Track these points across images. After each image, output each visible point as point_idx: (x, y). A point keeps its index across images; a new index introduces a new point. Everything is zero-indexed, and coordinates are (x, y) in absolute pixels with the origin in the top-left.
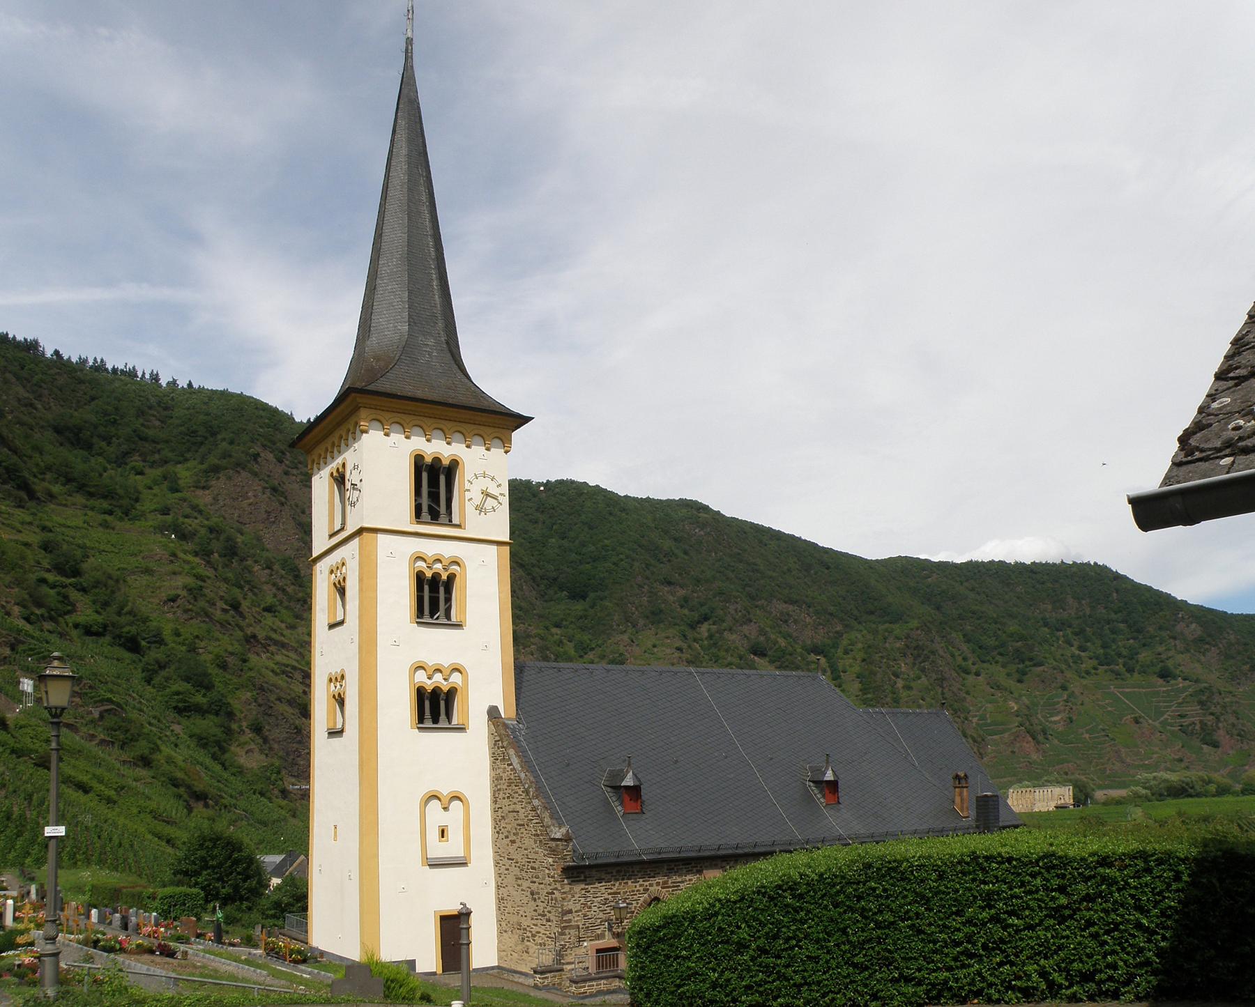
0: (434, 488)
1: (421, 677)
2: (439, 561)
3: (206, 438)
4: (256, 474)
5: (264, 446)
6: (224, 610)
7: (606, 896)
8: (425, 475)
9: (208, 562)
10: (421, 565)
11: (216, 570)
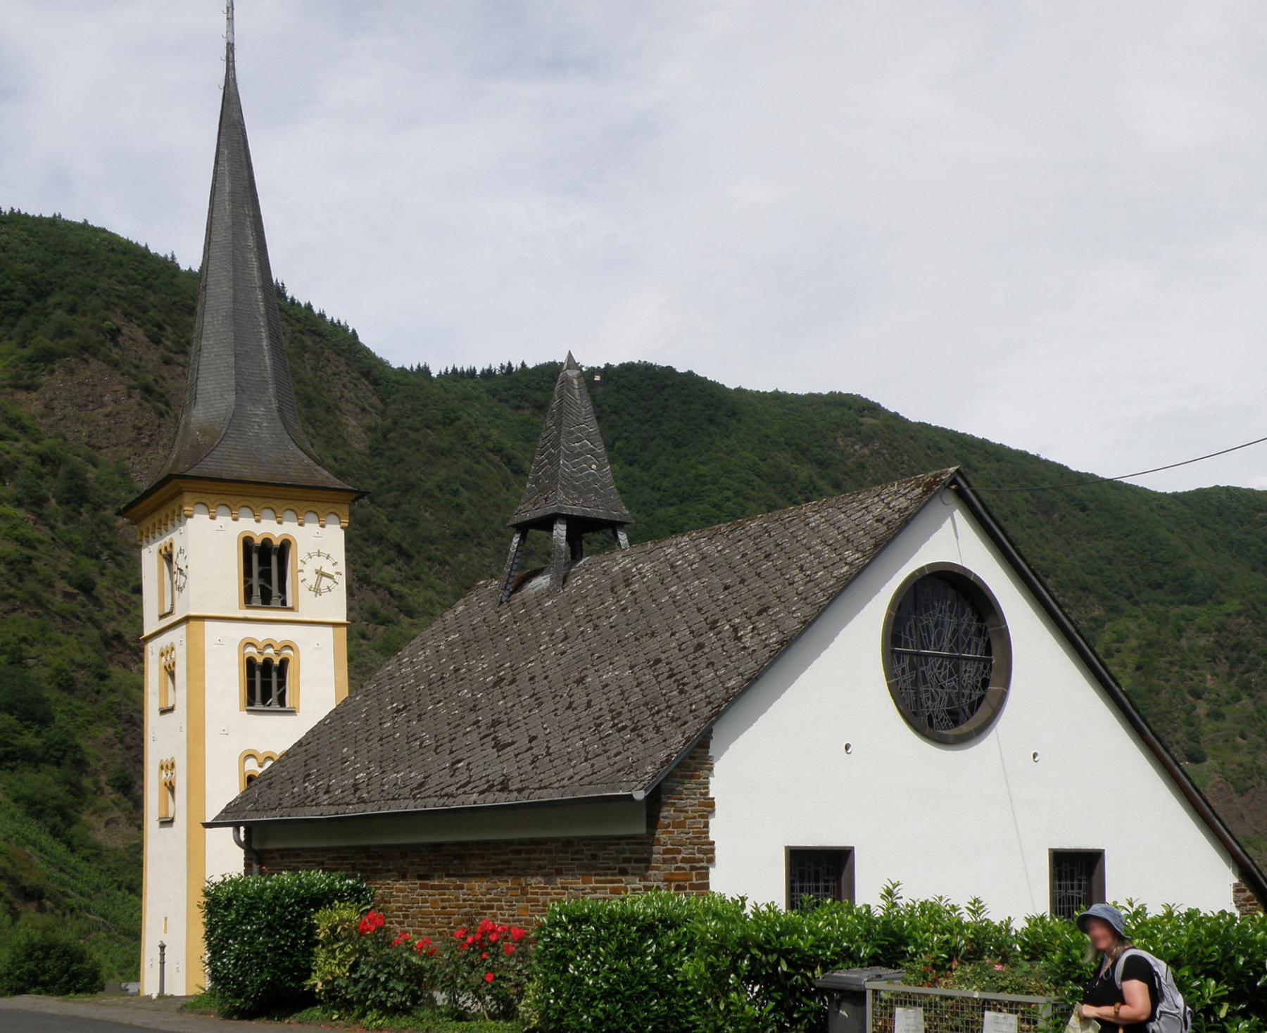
0: (265, 571)
2: (270, 645)
3: (28, 303)
4: (116, 365)
5: (128, 316)
6: (67, 595)
9: (40, 516)
10: (251, 651)
11: (52, 528)
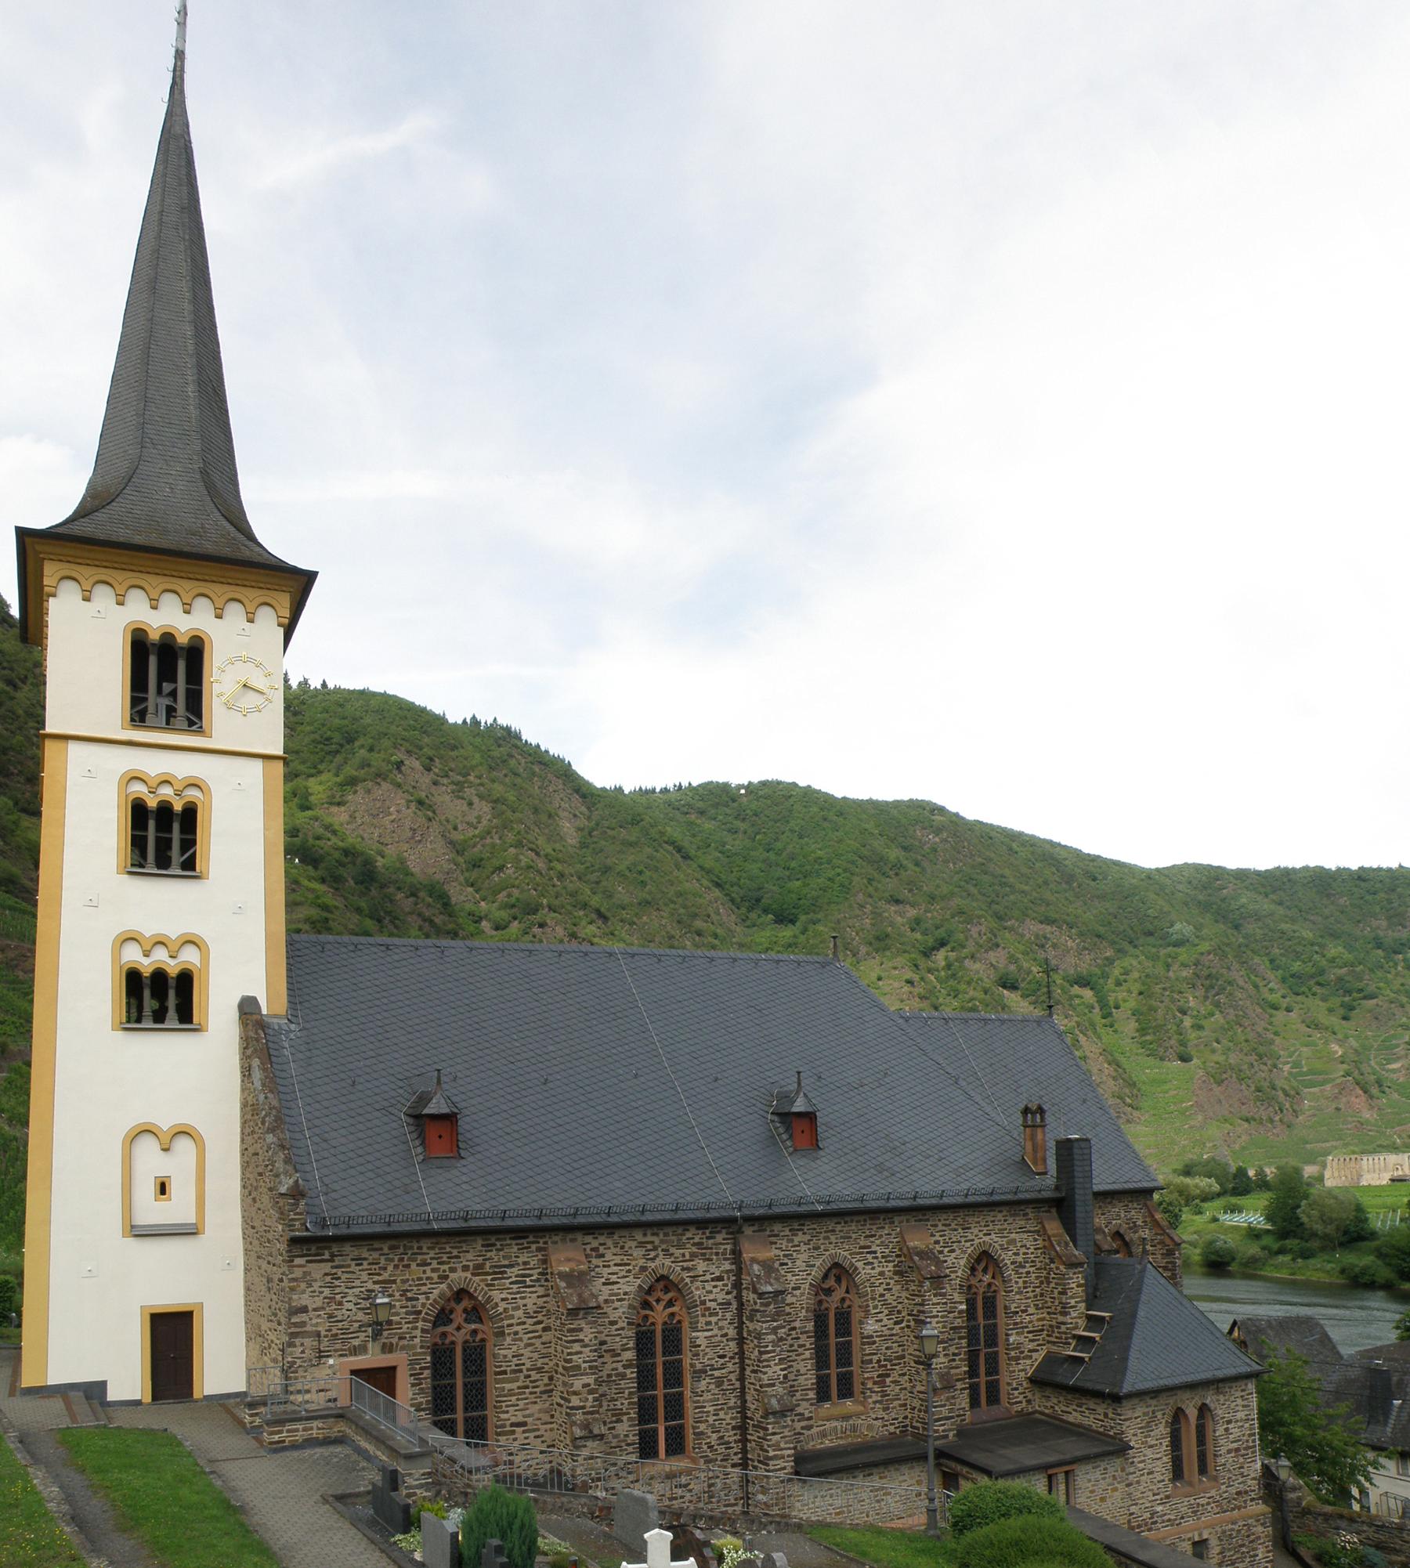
0: (167, 680)
1: (133, 955)
10: (139, 789)
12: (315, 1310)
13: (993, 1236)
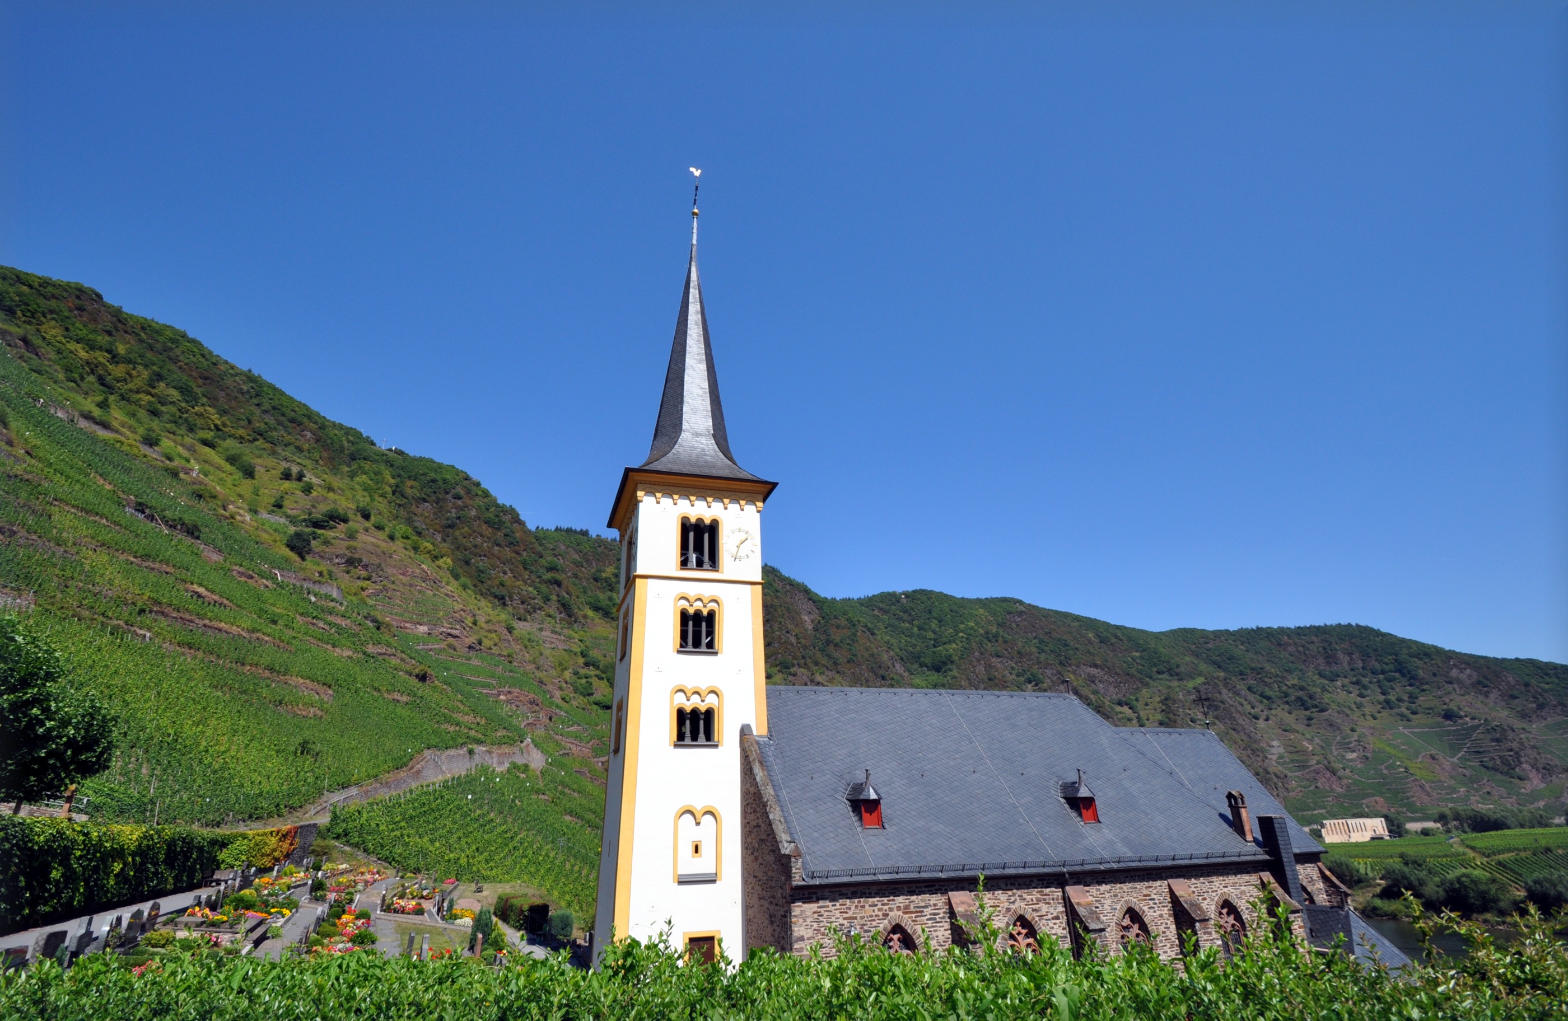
0: (700, 543)
1: (680, 700)
2: (700, 599)
7: (841, 921)
8: (691, 535)
12: (808, 939)
13: (1230, 888)
